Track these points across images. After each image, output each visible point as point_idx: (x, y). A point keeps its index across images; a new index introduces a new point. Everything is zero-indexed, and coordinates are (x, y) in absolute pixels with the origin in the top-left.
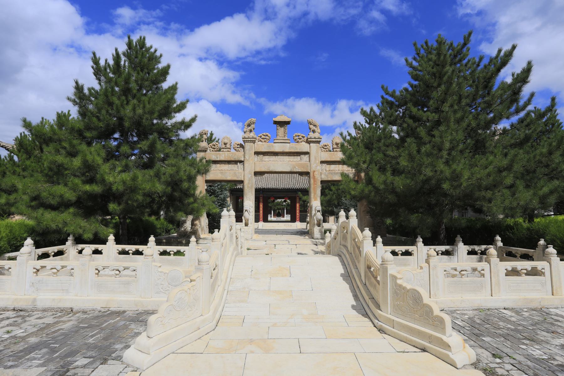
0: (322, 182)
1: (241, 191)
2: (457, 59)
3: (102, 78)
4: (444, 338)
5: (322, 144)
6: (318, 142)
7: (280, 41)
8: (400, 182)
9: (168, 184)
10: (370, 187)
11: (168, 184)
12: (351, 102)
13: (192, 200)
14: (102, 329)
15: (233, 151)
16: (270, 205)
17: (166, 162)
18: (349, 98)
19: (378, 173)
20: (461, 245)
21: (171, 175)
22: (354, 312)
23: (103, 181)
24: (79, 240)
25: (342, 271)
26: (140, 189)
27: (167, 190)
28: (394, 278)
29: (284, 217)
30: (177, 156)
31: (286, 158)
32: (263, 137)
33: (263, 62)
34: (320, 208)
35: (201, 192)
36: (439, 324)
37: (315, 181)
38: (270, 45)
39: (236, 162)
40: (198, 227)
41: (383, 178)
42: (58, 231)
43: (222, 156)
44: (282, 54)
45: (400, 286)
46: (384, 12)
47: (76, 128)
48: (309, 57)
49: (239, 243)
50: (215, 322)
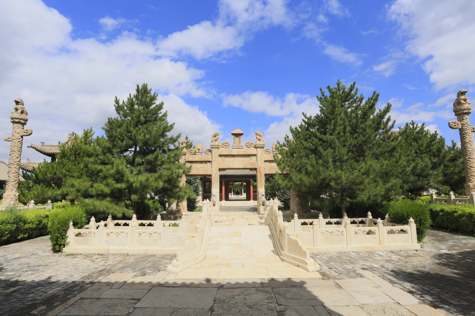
0: (265, 175)
1: (210, 181)
2: (348, 98)
3: (121, 112)
4: (306, 260)
5: (265, 149)
6: (263, 148)
7: (239, 43)
8: (307, 180)
9: (165, 182)
10: (292, 183)
11: (165, 182)
12: (298, 95)
13: (178, 190)
14: (149, 262)
15: (204, 154)
16: (230, 187)
17: (163, 166)
18: (295, 92)
19: (296, 174)
20: (346, 218)
21: (168, 176)
22: (272, 253)
23: (128, 181)
24: (114, 218)
25: (270, 234)
26: (150, 186)
27: (165, 185)
28: (288, 235)
29: (241, 195)
30: (170, 162)
31: (241, 159)
32: (225, 144)
33: (224, 62)
34: (264, 193)
35: (183, 184)
36: (304, 254)
37: (260, 174)
38: (230, 47)
39: (206, 162)
40: (181, 207)
41: (299, 176)
42: (104, 213)
43: (196, 158)
44: (240, 54)
45: (291, 238)
46: (328, 15)
47: (107, 147)
48: (262, 58)
49: (212, 218)
50: (204, 257)
